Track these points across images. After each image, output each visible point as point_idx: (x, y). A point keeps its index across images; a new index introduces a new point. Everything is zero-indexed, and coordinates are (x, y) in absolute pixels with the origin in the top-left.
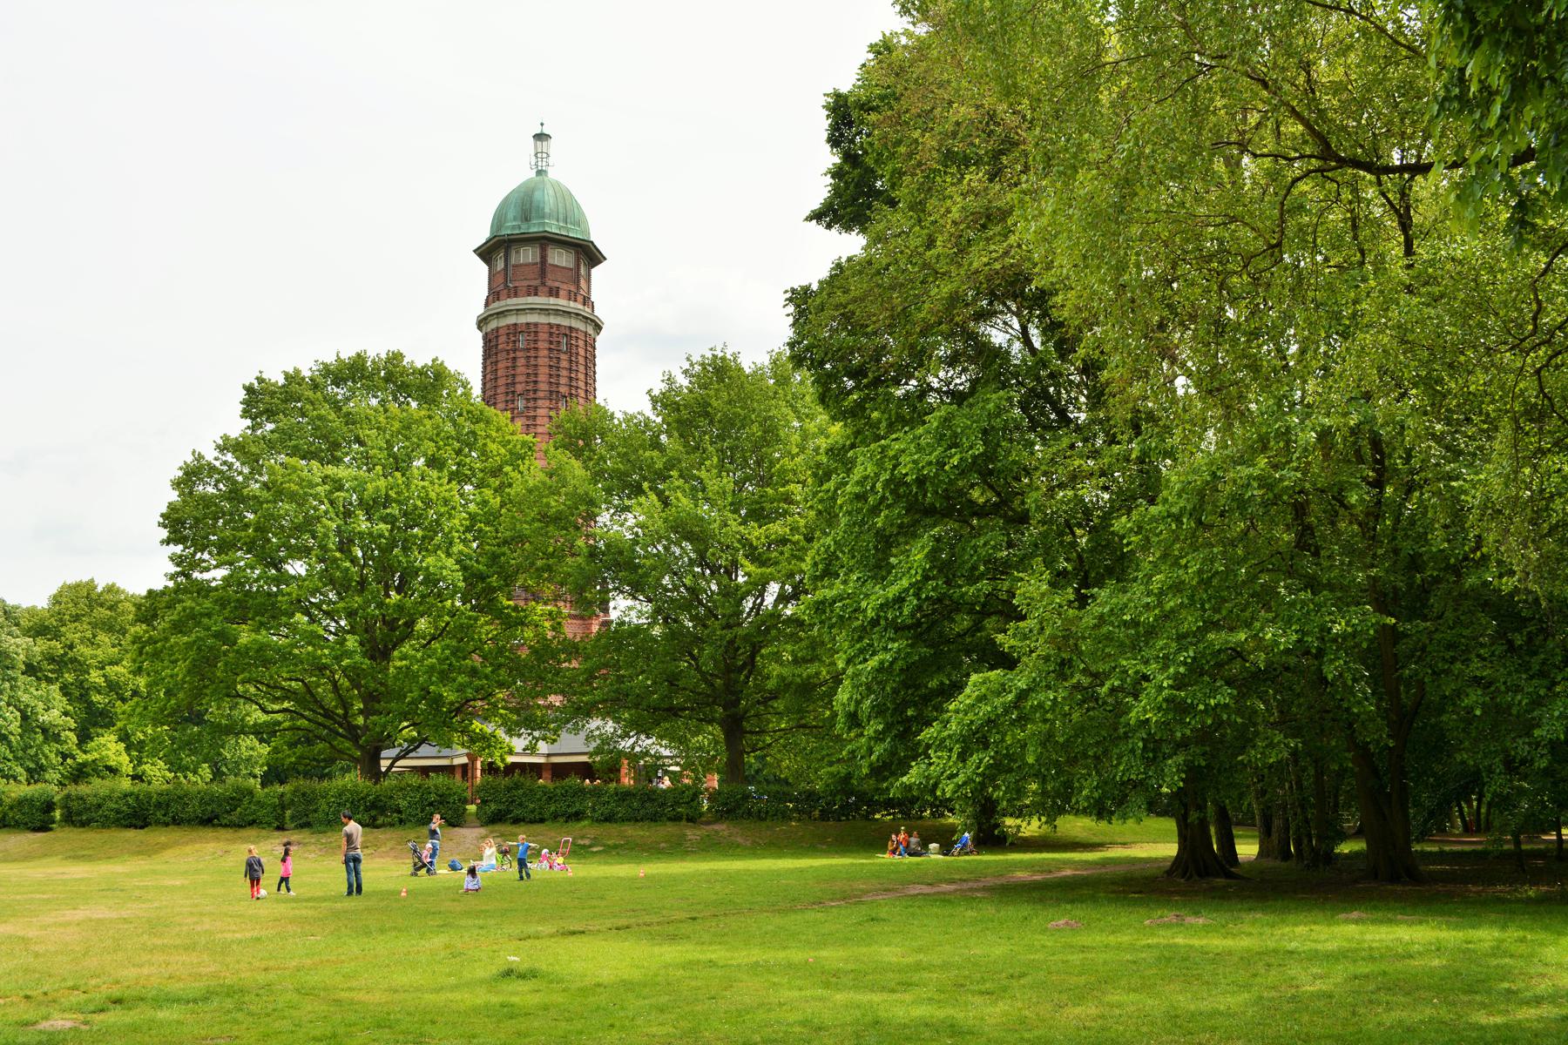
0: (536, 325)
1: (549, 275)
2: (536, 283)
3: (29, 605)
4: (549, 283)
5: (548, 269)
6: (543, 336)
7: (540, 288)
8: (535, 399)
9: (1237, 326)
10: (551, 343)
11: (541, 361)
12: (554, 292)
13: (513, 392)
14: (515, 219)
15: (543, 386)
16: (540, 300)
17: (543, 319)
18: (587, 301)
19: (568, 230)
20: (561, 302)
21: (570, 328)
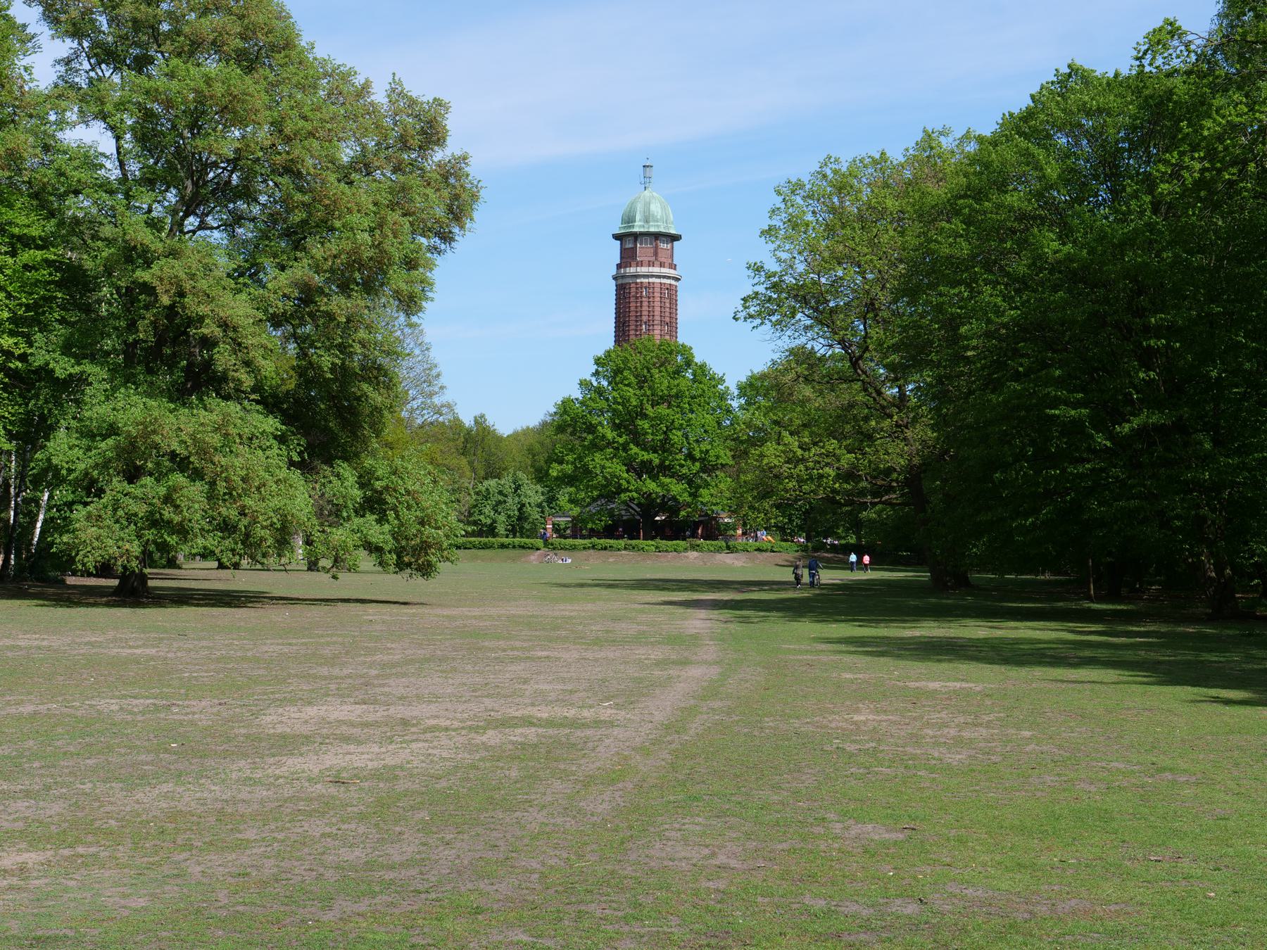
12: (662, 265)
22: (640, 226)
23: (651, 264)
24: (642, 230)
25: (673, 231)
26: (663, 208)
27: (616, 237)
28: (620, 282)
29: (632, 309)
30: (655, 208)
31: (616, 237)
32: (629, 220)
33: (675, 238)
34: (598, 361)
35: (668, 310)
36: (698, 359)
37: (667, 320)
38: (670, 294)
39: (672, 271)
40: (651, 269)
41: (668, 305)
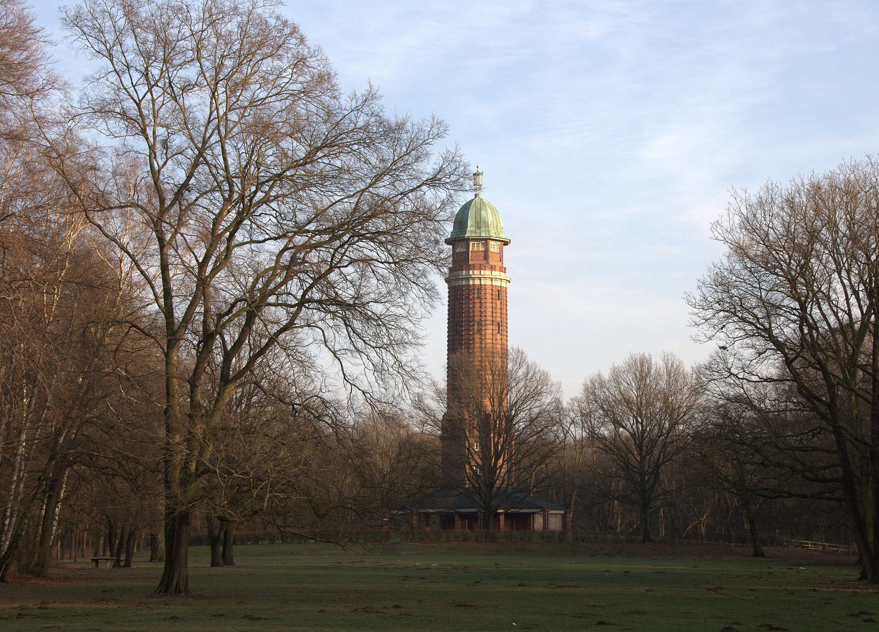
12: (492, 268)
18: (503, 270)
38: (500, 294)
41: (499, 306)
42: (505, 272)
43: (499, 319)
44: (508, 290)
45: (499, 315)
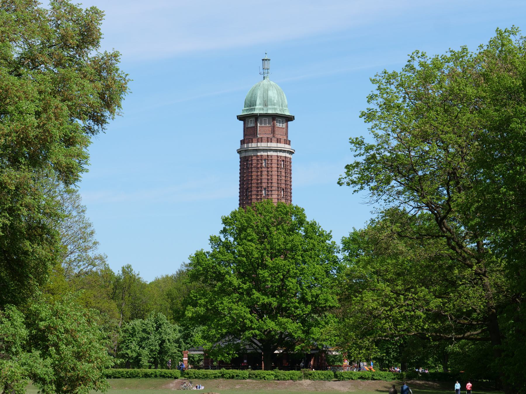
0: (271, 156)
1: (276, 133)
2: (271, 136)
3: (300, 206)
4: (276, 136)
5: (276, 129)
6: (275, 161)
7: (273, 139)
8: (271, 191)
9: (453, 274)
10: (268, 168)
11: (274, 173)
12: (278, 141)
13: (261, 187)
14: (260, 104)
15: (275, 185)
16: (273, 145)
17: (275, 154)
18: (288, 142)
19: (275, 109)
20: (281, 146)
21: (285, 157)
22: (260, 109)
23: (269, 140)
24: (262, 112)
25: (287, 113)
26: (279, 94)
27: (240, 118)
28: (244, 155)
29: (254, 177)
30: (273, 94)
31: (240, 118)
32: (251, 103)
33: (289, 119)
34: (225, 221)
35: (283, 178)
36: (309, 219)
37: (283, 186)
39: (281, 146)
40: (269, 144)
41: (283, 174)
42: (289, 144)
43: (283, 186)
44: (292, 160)
45: (283, 182)
